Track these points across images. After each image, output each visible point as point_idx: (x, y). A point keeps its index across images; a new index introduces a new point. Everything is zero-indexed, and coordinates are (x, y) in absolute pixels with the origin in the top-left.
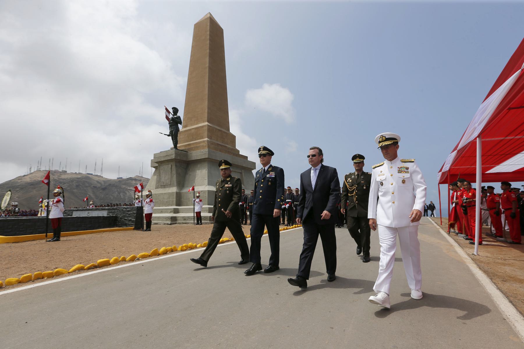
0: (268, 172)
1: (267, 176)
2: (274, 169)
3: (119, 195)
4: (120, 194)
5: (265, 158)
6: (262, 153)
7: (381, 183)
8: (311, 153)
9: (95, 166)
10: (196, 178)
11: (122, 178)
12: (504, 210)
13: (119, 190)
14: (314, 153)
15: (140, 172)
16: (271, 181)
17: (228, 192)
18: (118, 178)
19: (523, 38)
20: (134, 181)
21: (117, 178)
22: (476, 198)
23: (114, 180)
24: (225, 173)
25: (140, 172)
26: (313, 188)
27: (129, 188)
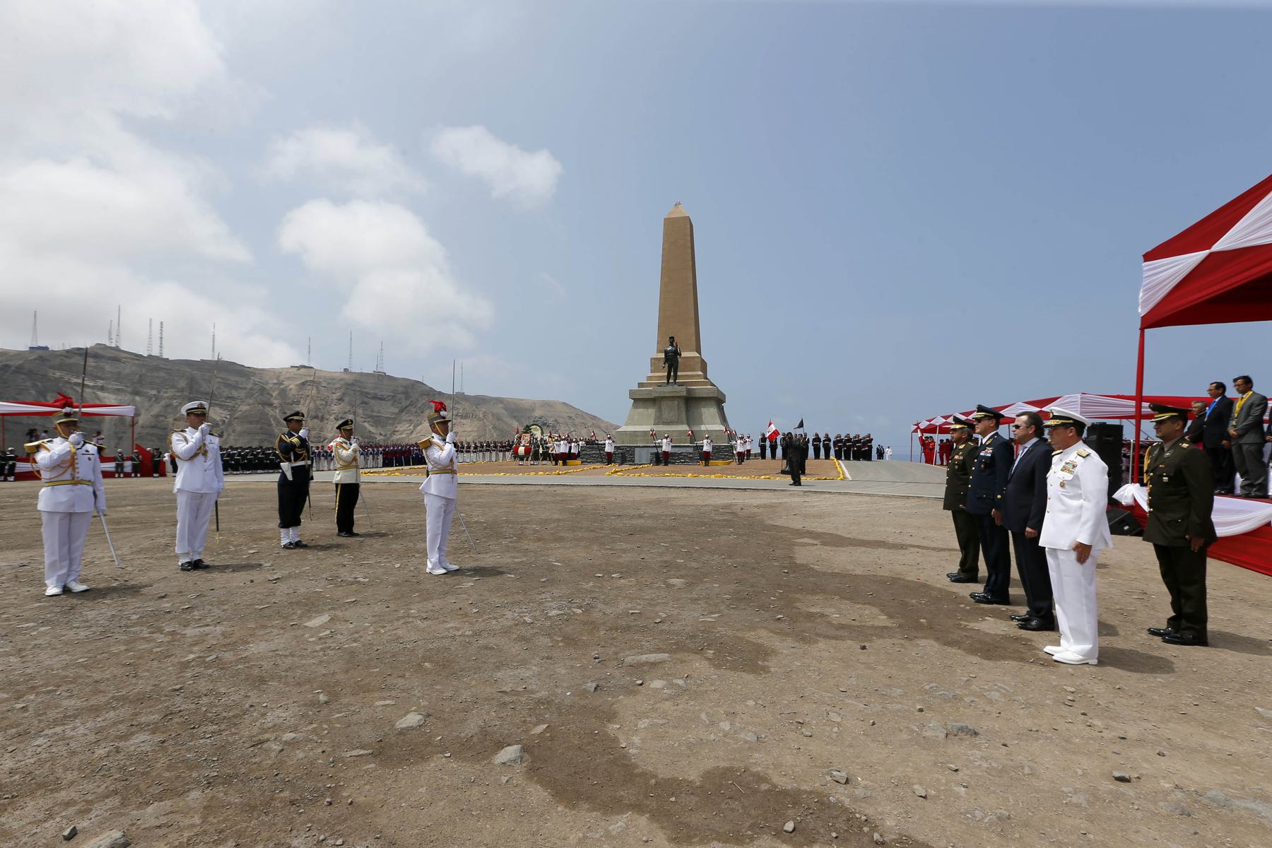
1: (981, 454)
9: (212, 352)
10: (704, 417)
11: (46, 348)
13: (39, 384)
15: (110, 333)
18: (30, 348)
19: (1269, 175)
21: (28, 349)
23: (19, 354)
25: (110, 333)
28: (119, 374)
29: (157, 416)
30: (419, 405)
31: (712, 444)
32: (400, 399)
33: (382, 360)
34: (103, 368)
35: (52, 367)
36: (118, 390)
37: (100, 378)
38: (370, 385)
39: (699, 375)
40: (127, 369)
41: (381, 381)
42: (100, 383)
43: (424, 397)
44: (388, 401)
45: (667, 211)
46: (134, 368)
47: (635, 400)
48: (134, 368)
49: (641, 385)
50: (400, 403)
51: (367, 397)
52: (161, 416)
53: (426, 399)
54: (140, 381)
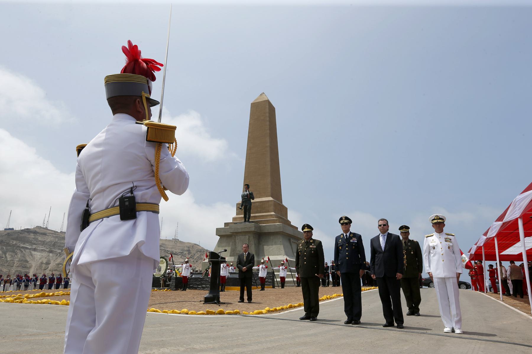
0: (350, 238)
2: (355, 235)
3: (4, 256)
4: (5, 254)
5: (347, 226)
6: (345, 222)
7: (434, 248)
8: (382, 223)
11: (13, 229)
12: (517, 294)
14: (385, 224)
15: (44, 220)
16: (354, 246)
17: (313, 252)
20: (32, 234)
22: (479, 291)
24: (308, 235)
25: (44, 220)
26: (383, 250)
27: (22, 245)
28: (44, 242)
29: (58, 264)
30: (195, 258)
31: (266, 270)
32: (185, 254)
33: (177, 230)
34: (37, 239)
35: (13, 239)
36: (42, 250)
37: (34, 244)
38: (170, 246)
39: (271, 215)
40: (48, 239)
41: (176, 244)
42: (34, 246)
43: (199, 253)
44: (179, 255)
45: (254, 98)
46: (52, 239)
47: (222, 236)
48: (52, 239)
49: (226, 224)
50: (185, 256)
51: (168, 253)
52: (61, 264)
53: (200, 254)
54: (54, 245)
